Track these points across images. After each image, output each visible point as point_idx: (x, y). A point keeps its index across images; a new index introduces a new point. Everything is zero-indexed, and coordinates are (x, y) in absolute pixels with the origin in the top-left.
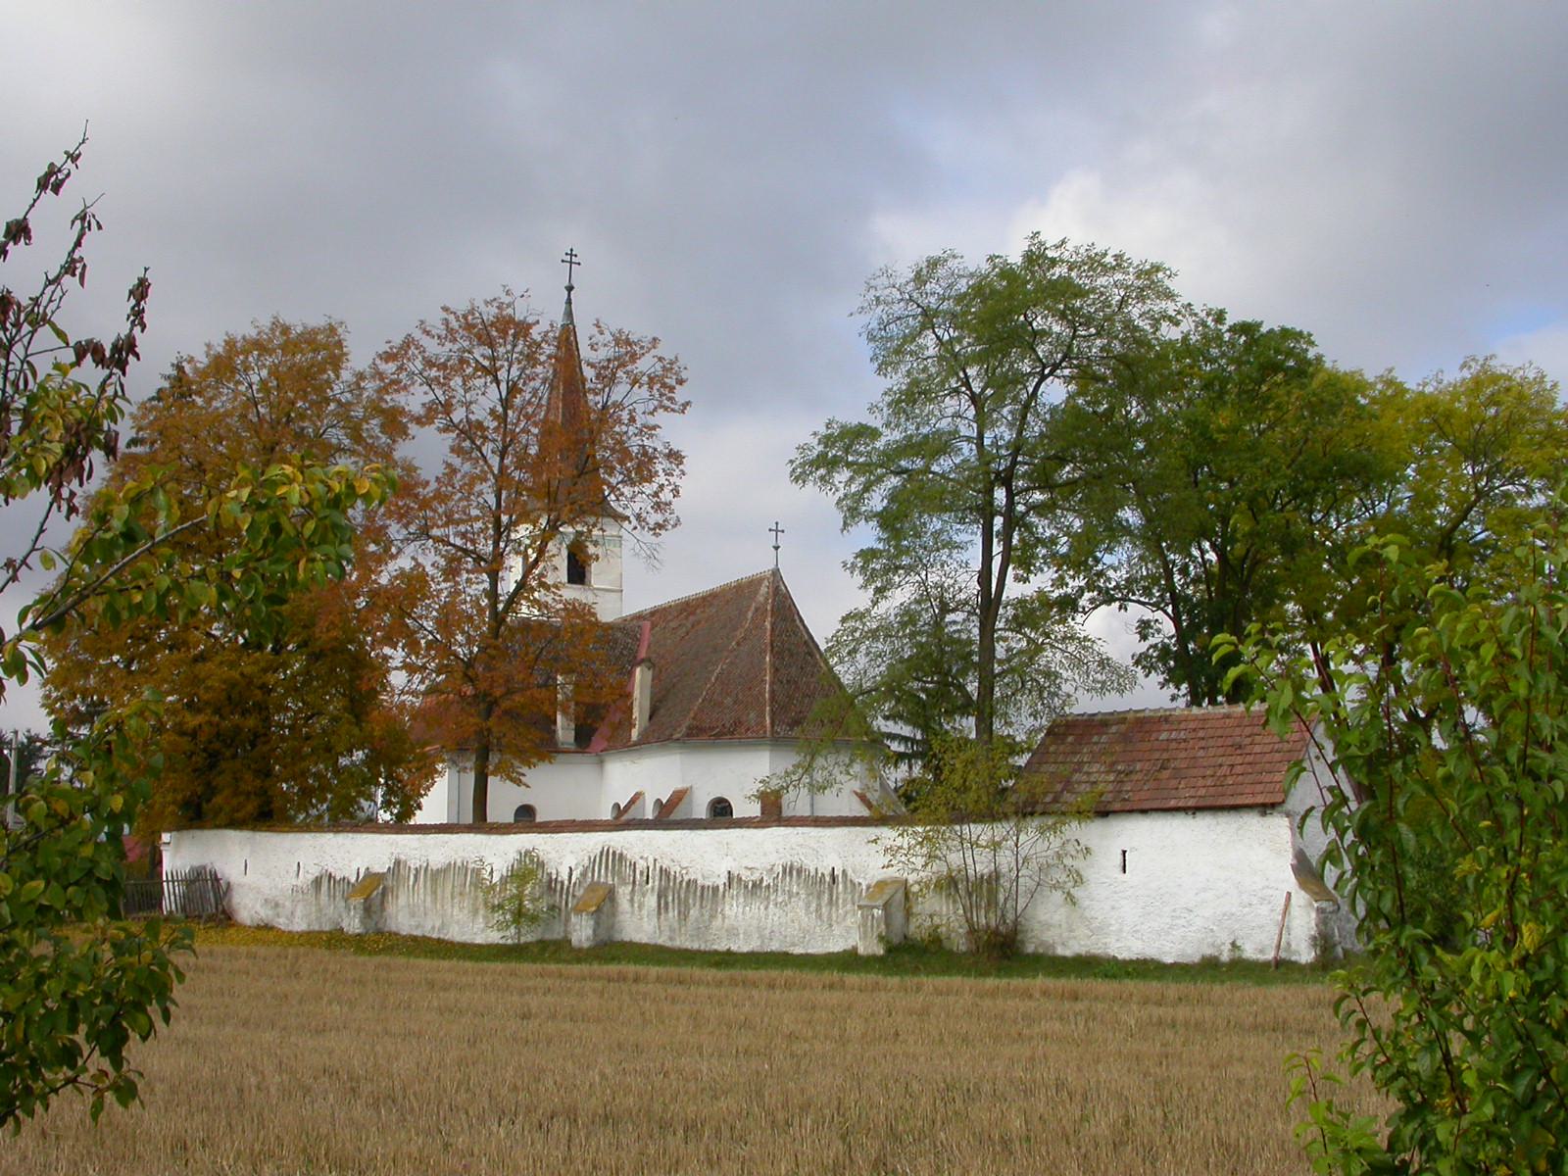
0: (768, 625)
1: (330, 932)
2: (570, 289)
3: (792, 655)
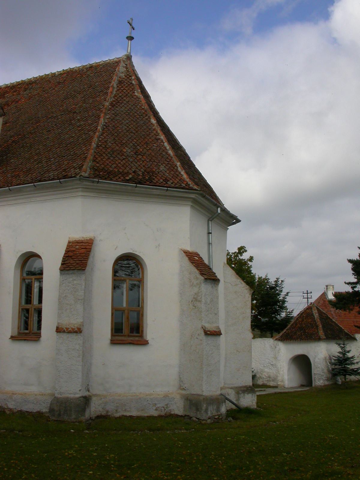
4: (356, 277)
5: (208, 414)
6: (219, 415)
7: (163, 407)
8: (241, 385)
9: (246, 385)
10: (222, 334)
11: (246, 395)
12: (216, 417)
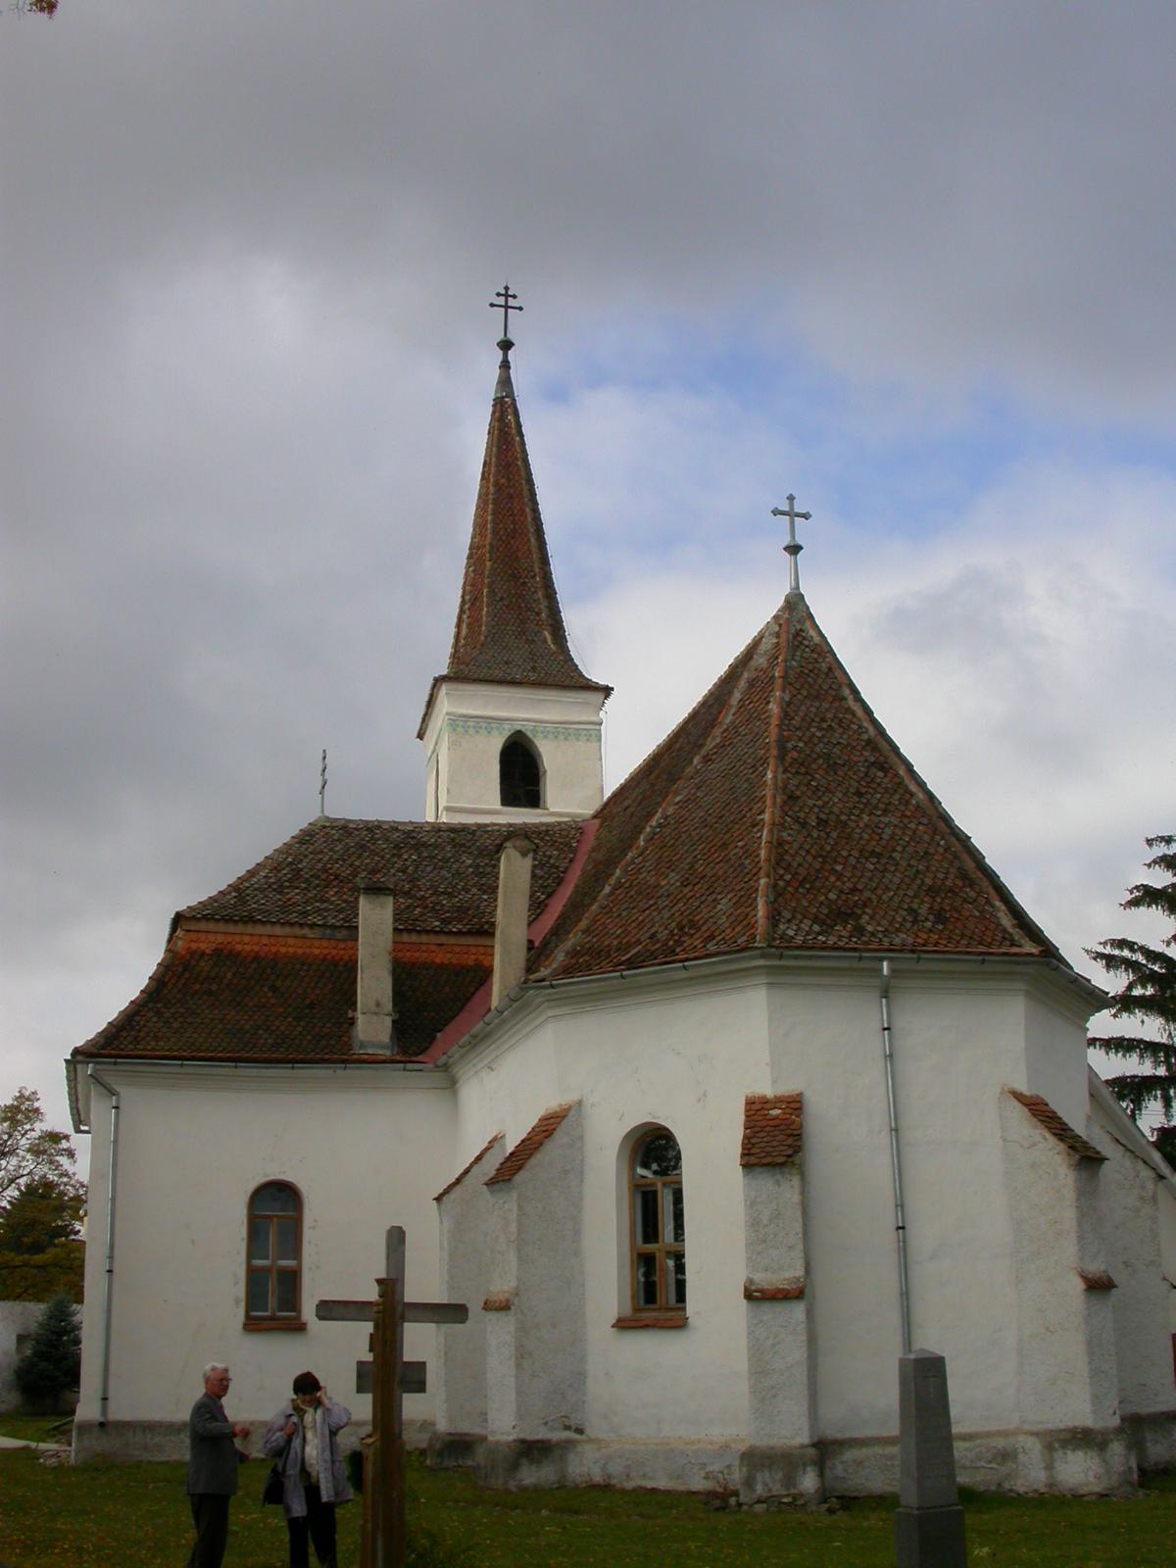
0: (774, 708)
1: (400, 1437)
2: (506, 345)
3: (833, 767)
4: (1147, 1098)
5: (755, 1490)
6: (795, 1497)
7: (722, 1472)
8: (1062, 1426)
9: (1076, 1424)
10: (1115, 1286)
11: (1069, 1452)
12: (785, 1500)
